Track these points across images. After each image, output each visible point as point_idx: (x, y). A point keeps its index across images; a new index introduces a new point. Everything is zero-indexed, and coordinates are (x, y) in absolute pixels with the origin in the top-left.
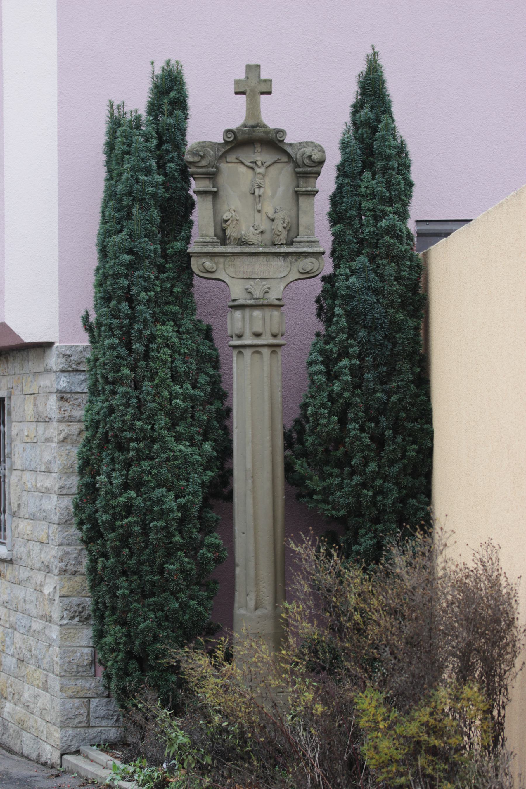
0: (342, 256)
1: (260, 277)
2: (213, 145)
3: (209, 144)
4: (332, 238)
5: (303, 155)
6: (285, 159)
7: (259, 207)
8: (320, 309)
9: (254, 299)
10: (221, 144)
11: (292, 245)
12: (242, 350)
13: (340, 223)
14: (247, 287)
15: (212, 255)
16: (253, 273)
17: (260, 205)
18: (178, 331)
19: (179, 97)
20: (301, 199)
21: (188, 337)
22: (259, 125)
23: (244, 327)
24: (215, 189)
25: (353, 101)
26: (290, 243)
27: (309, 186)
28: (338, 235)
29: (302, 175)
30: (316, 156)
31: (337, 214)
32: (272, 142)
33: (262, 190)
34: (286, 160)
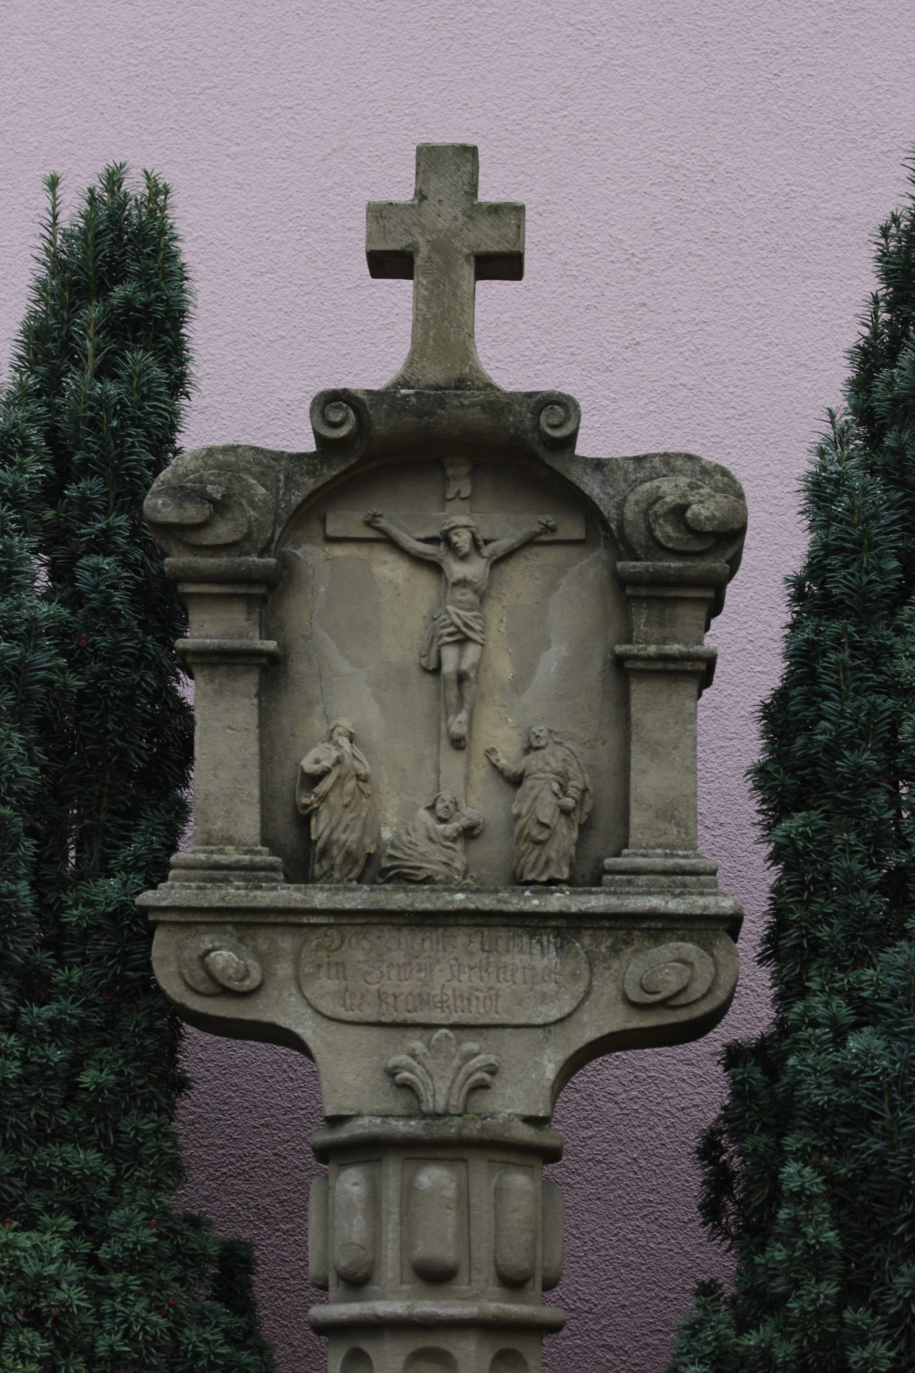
0: (816, 946)
1: (454, 1018)
2: (268, 462)
3: (249, 455)
4: (772, 875)
5: (651, 505)
6: (572, 529)
7: (457, 724)
8: (720, 1182)
9: (424, 1116)
10: (300, 457)
11: (598, 882)
12: (365, 1345)
13: (809, 808)
14: (394, 1061)
15: (246, 921)
16: (423, 1000)
17: (463, 716)
18: (92, 1260)
19: (147, 305)
20: (640, 693)
21: (134, 1282)
22: (469, 382)
23: (376, 1238)
24: (271, 645)
25: (854, 333)
26: (594, 878)
27: (676, 640)
28: (797, 853)
29: (643, 592)
30: (705, 509)
31: (791, 771)
32: (517, 451)
33: (472, 652)
34: (578, 533)
